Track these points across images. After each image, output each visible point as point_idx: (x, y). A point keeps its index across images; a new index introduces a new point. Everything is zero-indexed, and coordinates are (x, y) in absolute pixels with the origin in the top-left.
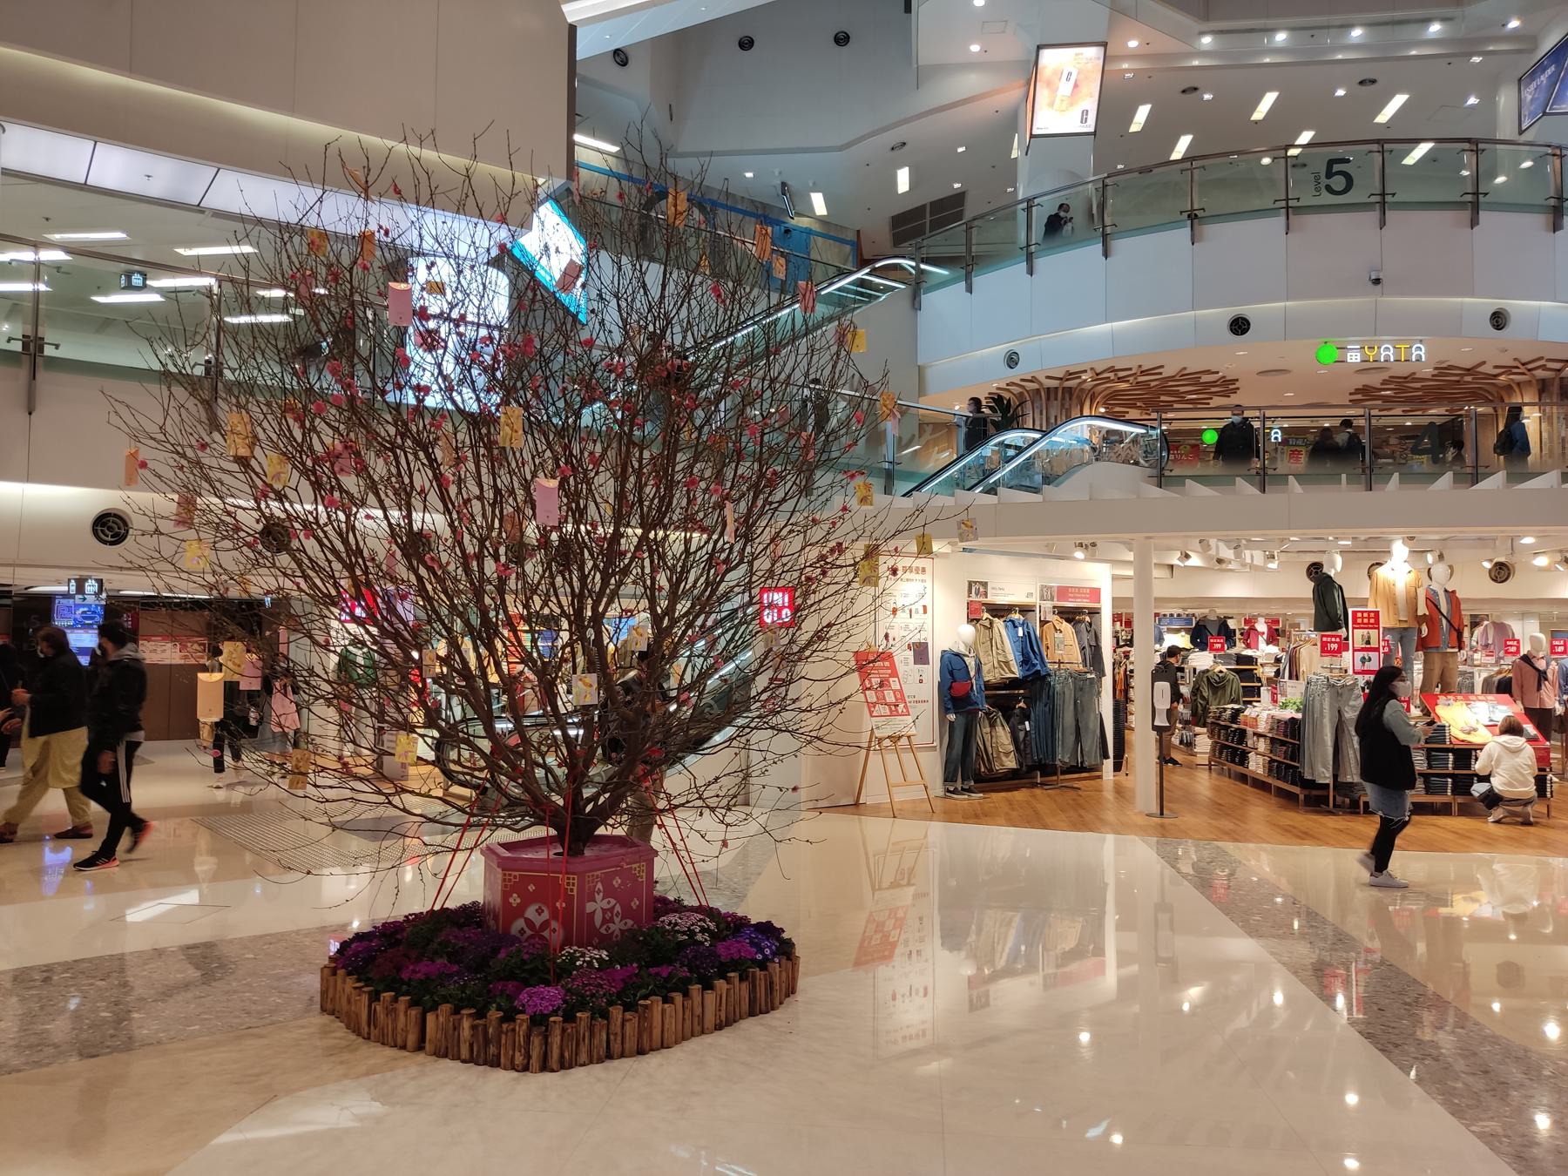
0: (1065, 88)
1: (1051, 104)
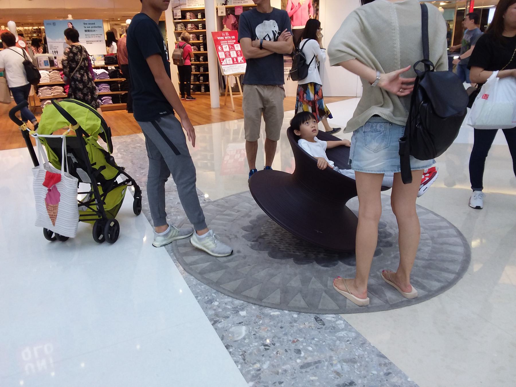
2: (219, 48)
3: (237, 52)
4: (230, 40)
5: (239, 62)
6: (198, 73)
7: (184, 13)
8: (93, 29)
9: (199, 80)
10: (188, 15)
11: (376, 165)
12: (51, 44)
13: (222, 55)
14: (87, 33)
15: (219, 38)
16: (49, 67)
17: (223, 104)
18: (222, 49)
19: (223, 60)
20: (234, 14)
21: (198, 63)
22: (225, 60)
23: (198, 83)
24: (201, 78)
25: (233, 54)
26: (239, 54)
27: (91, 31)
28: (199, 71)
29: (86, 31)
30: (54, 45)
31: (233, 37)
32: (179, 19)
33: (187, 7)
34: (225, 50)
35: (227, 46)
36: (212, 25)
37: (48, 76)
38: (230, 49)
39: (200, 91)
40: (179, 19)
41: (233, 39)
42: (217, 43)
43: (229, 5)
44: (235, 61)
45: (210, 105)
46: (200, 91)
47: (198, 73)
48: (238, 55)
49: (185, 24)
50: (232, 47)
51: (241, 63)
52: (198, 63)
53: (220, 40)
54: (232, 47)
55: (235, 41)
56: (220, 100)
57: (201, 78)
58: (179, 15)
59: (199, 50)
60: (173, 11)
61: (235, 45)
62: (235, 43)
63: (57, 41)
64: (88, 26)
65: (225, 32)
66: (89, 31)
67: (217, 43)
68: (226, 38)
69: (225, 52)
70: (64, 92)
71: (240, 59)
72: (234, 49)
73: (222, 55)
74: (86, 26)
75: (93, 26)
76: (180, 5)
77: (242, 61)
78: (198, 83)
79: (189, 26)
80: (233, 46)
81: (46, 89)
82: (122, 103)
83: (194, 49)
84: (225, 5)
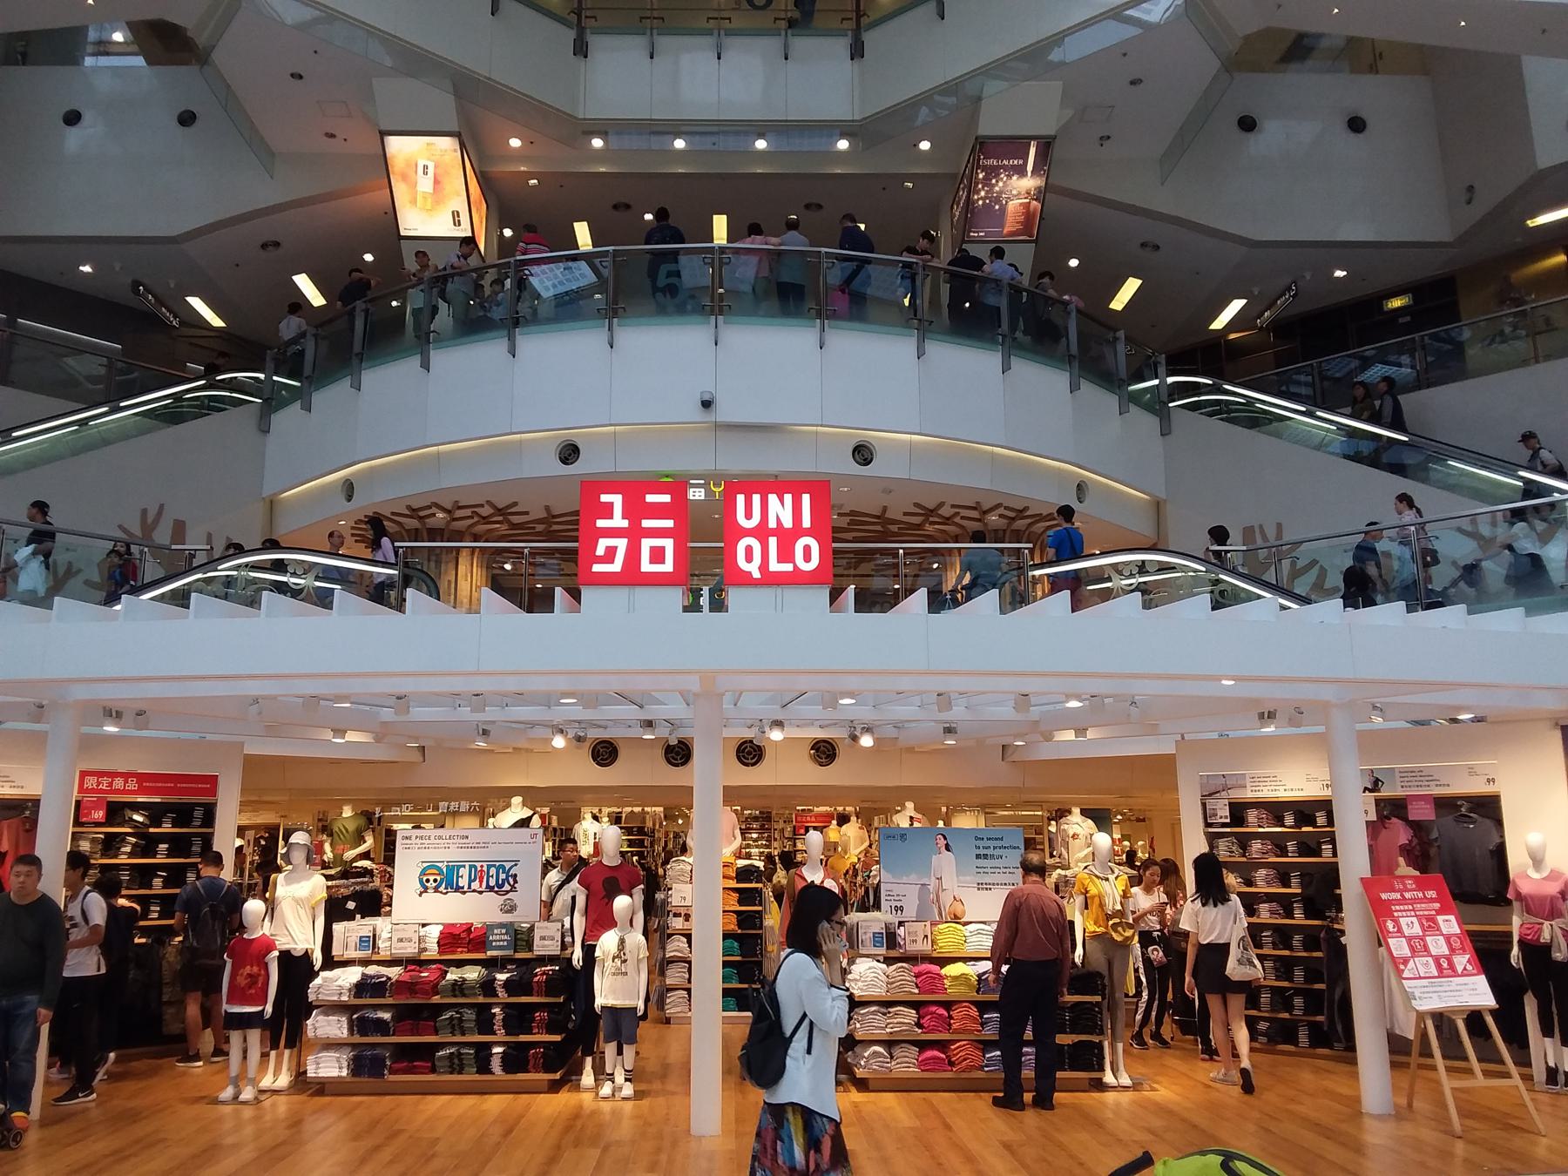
0: (425, 185)
1: (414, 202)
2: (1390, 925)
3: (1448, 938)
4: (1420, 901)
5: (1460, 969)
6: (1285, 984)
7: (1238, 812)
8: (997, 852)
9: (1289, 1007)
10: (1252, 815)
11: (183, 735)
12: (889, 886)
13: (1399, 947)
14: (981, 862)
15: (1384, 896)
16: (882, 951)
17: (1403, 1101)
18: (1400, 930)
19: (1406, 961)
20: (1405, 819)
21: (1287, 953)
22: (1411, 964)
23: (1286, 1015)
24: (1298, 1001)
25: (1438, 946)
26: (1457, 945)
27: (992, 857)
28: (1290, 980)
29: (978, 856)
30: (897, 889)
31: (1432, 894)
32: (1224, 825)
33: (1249, 794)
34: (1407, 932)
35: (1415, 920)
36: (1353, 858)
37: (884, 978)
38: (1424, 930)
39: (1295, 1042)
40: (1224, 825)
41: (1432, 900)
42: (1381, 910)
43: (1385, 793)
44: (1445, 969)
45: (1357, 1100)
46: (1295, 1042)
47: (1285, 984)
48: (1452, 950)
49: (1244, 842)
50: (1430, 925)
51: (1465, 973)
52: (1287, 953)
53: (1390, 902)
54: (1430, 925)
55: (1437, 905)
56: (1396, 1088)
57: (1298, 1001)
58: (1224, 813)
59: (1290, 915)
60: (1204, 805)
61: (1440, 918)
62: (1439, 912)
63: (905, 880)
64: (992, 844)
65: (1403, 877)
66: (985, 856)
67: (1381, 910)
68: (1407, 895)
69: (1409, 939)
70: (918, 1025)
71: (1462, 961)
72: (1439, 929)
73: (1401, 948)
74: (979, 843)
75: (999, 843)
76: (1226, 788)
77: (1469, 967)
78: (1286, 1015)
79: (1256, 846)
80: (1432, 919)
81: (873, 1013)
82: (1073, 1069)
83: (1272, 912)
84: (1371, 791)
